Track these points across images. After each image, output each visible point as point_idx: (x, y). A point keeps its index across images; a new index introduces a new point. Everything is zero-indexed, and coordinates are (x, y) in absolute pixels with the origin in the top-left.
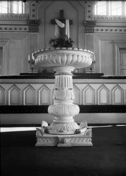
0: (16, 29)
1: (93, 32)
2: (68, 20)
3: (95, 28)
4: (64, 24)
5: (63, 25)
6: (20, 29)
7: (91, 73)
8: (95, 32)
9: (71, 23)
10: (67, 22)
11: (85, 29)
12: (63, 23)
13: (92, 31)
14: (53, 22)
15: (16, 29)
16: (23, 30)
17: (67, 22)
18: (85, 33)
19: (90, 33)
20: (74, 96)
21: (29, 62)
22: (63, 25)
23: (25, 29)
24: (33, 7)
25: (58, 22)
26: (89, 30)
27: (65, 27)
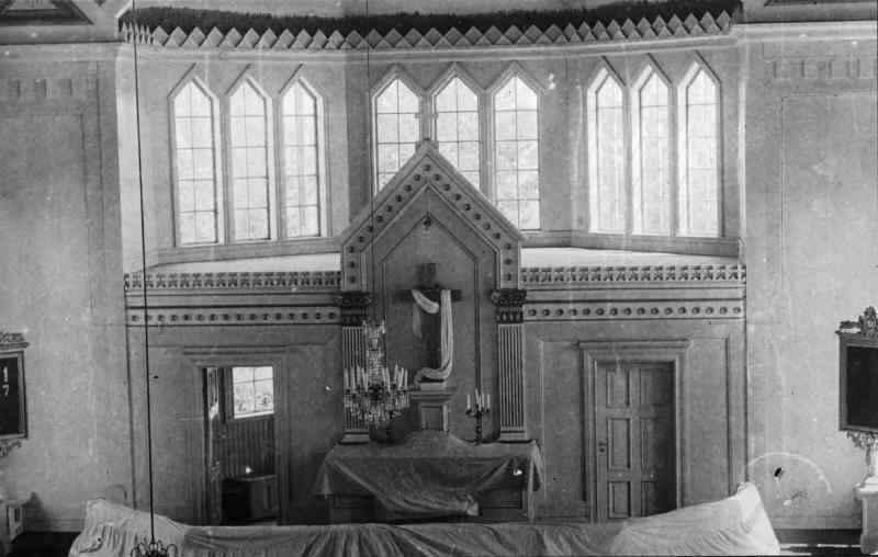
0: (186, 317)
1: (521, 321)
2: (449, 292)
3: (525, 308)
4: (436, 305)
5: (433, 307)
6: (575, 312)
7: (456, 487)
8: (525, 318)
9: (456, 296)
10: (446, 297)
11: (497, 312)
12: (434, 301)
13: (518, 317)
14: (406, 297)
15: (587, 312)
16: (539, 316)
17: (446, 297)
18: (498, 322)
19: (511, 322)
20: (219, 509)
21: (469, 412)
22: (433, 307)
23: (331, 315)
24: (507, 266)
25: (417, 295)
26: (507, 314)
27: (439, 312)
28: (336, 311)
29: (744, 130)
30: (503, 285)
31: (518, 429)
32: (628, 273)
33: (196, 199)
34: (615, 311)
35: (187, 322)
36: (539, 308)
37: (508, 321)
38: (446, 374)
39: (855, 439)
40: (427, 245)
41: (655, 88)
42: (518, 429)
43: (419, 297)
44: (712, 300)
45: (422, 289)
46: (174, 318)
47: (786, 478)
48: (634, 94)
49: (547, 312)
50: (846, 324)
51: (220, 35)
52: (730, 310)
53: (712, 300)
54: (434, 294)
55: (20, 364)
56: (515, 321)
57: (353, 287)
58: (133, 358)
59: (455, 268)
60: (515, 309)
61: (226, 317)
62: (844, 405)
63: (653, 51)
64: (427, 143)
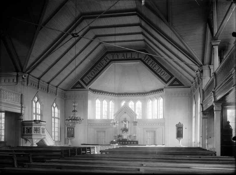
5: (125, 123)
9: (129, 122)
10: (127, 122)
14: (122, 122)
17: (127, 122)
22: (125, 123)
30: (134, 121)
31: (29, 134)
32: (161, 120)
33: (156, 105)
34: (95, 125)
36: (139, 124)
40: (125, 116)
41: (156, 100)
42: (29, 134)
43: (124, 122)
45: (124, 121)
46: (92, 125)
47: (209, 138)
48: (159, 101)
49: (98, 125)
50: (177, 124)
54: (125, 121)
59: (128, 118)
63: (161, 95)
64: (152, 101)
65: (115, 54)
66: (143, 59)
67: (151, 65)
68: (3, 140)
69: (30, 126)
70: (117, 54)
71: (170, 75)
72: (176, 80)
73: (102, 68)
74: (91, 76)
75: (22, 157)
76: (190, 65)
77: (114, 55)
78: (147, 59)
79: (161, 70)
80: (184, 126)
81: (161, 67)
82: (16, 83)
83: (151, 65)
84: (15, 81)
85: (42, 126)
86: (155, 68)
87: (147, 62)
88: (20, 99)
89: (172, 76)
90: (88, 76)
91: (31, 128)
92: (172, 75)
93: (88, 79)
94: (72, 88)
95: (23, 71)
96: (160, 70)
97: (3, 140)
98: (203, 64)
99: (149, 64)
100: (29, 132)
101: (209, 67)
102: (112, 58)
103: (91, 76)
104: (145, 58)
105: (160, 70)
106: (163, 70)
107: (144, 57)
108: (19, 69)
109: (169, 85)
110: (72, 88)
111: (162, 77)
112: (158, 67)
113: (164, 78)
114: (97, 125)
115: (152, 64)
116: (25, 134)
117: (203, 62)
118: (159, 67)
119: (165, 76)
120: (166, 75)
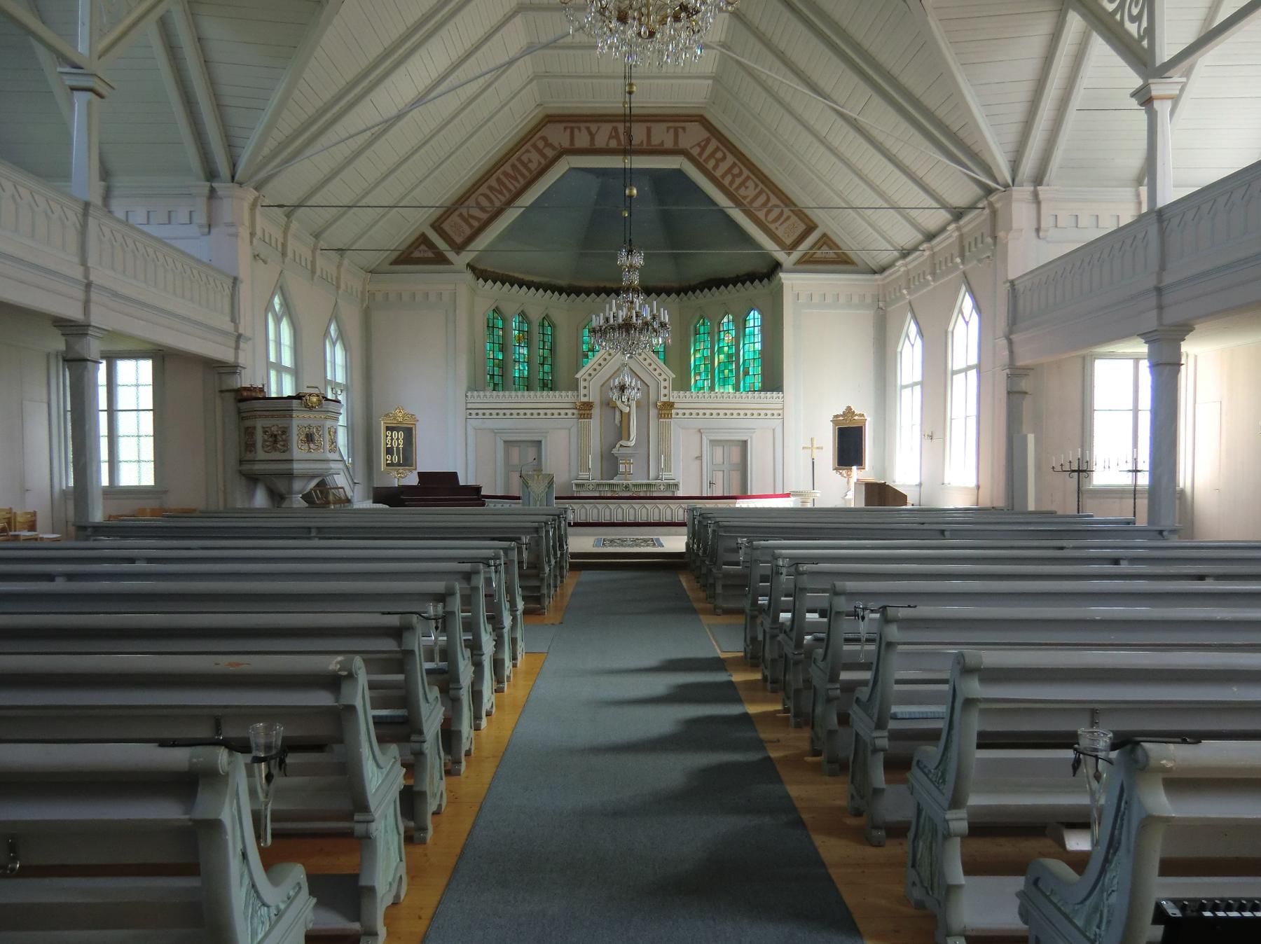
1: (671, 418)
3: (674, 412)
16: (722, 416)
27: (629, 412)
28: (575, 411)
29: (263, 468)
35: (553, 417)
37: (664, 418)
38: (632, 443)
39: (841, 473)
44: (753, 409)
51: (492, 284)
52: (735, 414)
53: (753, 409)
55: (414, 431)
56: (668, 418)
57: (586, 400)
58: (469, 462)
60: (588, 412)
61: (532, 414)
62: (114, 375)
65: (579, 128)
66: (695, 152)
67: (729, 178)
68: (148, 479)
69: (280, 422)
70: (588, 129)
71: (802, 220)
72: (825, 240)
73: (522, 181)
74: (476, 212)
75: (749, 590)
76: (138, 226)
77: (576, 132)
78: (712, 155)
79: (768, 199)
80: (867, 423)
81: (766, 190)
82: (207, 230)
83: (729, 178)
84: (201, 218)
85: (260, 416)
86: (742, 191)
87: (710, 165)
88: (227, 302)
89: (811, 228)
90: (465, 214)
91: (285, 431)
92: (417, 239)
93: (463, 224)
94: (396, 262)
95: (237, 178)
96: (763, 199)
97: (148, 479)
98: (1013, 181)
99: (718, 174)
100: (275, 449)
101: (1036, 195)
102: (566, 144)
103: (476, 212)
104: (703, 149)
105: (763, 199)
106: (774, 200)
107: (698, 144)
108: (223, 168)
109: (800, 261)
110: (396, 262)
111: (772, 227)
112: (757, 186)
113: (780, 233)
114: (705, 414)
115: (734, 176)
116: (261, 454)
117: (1015, 166)
118: (761, 185)
119: (785, 225)
120: (788, 222)
